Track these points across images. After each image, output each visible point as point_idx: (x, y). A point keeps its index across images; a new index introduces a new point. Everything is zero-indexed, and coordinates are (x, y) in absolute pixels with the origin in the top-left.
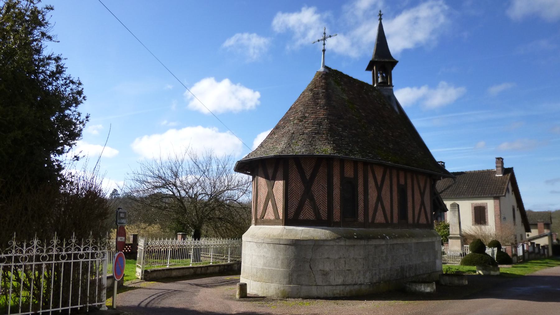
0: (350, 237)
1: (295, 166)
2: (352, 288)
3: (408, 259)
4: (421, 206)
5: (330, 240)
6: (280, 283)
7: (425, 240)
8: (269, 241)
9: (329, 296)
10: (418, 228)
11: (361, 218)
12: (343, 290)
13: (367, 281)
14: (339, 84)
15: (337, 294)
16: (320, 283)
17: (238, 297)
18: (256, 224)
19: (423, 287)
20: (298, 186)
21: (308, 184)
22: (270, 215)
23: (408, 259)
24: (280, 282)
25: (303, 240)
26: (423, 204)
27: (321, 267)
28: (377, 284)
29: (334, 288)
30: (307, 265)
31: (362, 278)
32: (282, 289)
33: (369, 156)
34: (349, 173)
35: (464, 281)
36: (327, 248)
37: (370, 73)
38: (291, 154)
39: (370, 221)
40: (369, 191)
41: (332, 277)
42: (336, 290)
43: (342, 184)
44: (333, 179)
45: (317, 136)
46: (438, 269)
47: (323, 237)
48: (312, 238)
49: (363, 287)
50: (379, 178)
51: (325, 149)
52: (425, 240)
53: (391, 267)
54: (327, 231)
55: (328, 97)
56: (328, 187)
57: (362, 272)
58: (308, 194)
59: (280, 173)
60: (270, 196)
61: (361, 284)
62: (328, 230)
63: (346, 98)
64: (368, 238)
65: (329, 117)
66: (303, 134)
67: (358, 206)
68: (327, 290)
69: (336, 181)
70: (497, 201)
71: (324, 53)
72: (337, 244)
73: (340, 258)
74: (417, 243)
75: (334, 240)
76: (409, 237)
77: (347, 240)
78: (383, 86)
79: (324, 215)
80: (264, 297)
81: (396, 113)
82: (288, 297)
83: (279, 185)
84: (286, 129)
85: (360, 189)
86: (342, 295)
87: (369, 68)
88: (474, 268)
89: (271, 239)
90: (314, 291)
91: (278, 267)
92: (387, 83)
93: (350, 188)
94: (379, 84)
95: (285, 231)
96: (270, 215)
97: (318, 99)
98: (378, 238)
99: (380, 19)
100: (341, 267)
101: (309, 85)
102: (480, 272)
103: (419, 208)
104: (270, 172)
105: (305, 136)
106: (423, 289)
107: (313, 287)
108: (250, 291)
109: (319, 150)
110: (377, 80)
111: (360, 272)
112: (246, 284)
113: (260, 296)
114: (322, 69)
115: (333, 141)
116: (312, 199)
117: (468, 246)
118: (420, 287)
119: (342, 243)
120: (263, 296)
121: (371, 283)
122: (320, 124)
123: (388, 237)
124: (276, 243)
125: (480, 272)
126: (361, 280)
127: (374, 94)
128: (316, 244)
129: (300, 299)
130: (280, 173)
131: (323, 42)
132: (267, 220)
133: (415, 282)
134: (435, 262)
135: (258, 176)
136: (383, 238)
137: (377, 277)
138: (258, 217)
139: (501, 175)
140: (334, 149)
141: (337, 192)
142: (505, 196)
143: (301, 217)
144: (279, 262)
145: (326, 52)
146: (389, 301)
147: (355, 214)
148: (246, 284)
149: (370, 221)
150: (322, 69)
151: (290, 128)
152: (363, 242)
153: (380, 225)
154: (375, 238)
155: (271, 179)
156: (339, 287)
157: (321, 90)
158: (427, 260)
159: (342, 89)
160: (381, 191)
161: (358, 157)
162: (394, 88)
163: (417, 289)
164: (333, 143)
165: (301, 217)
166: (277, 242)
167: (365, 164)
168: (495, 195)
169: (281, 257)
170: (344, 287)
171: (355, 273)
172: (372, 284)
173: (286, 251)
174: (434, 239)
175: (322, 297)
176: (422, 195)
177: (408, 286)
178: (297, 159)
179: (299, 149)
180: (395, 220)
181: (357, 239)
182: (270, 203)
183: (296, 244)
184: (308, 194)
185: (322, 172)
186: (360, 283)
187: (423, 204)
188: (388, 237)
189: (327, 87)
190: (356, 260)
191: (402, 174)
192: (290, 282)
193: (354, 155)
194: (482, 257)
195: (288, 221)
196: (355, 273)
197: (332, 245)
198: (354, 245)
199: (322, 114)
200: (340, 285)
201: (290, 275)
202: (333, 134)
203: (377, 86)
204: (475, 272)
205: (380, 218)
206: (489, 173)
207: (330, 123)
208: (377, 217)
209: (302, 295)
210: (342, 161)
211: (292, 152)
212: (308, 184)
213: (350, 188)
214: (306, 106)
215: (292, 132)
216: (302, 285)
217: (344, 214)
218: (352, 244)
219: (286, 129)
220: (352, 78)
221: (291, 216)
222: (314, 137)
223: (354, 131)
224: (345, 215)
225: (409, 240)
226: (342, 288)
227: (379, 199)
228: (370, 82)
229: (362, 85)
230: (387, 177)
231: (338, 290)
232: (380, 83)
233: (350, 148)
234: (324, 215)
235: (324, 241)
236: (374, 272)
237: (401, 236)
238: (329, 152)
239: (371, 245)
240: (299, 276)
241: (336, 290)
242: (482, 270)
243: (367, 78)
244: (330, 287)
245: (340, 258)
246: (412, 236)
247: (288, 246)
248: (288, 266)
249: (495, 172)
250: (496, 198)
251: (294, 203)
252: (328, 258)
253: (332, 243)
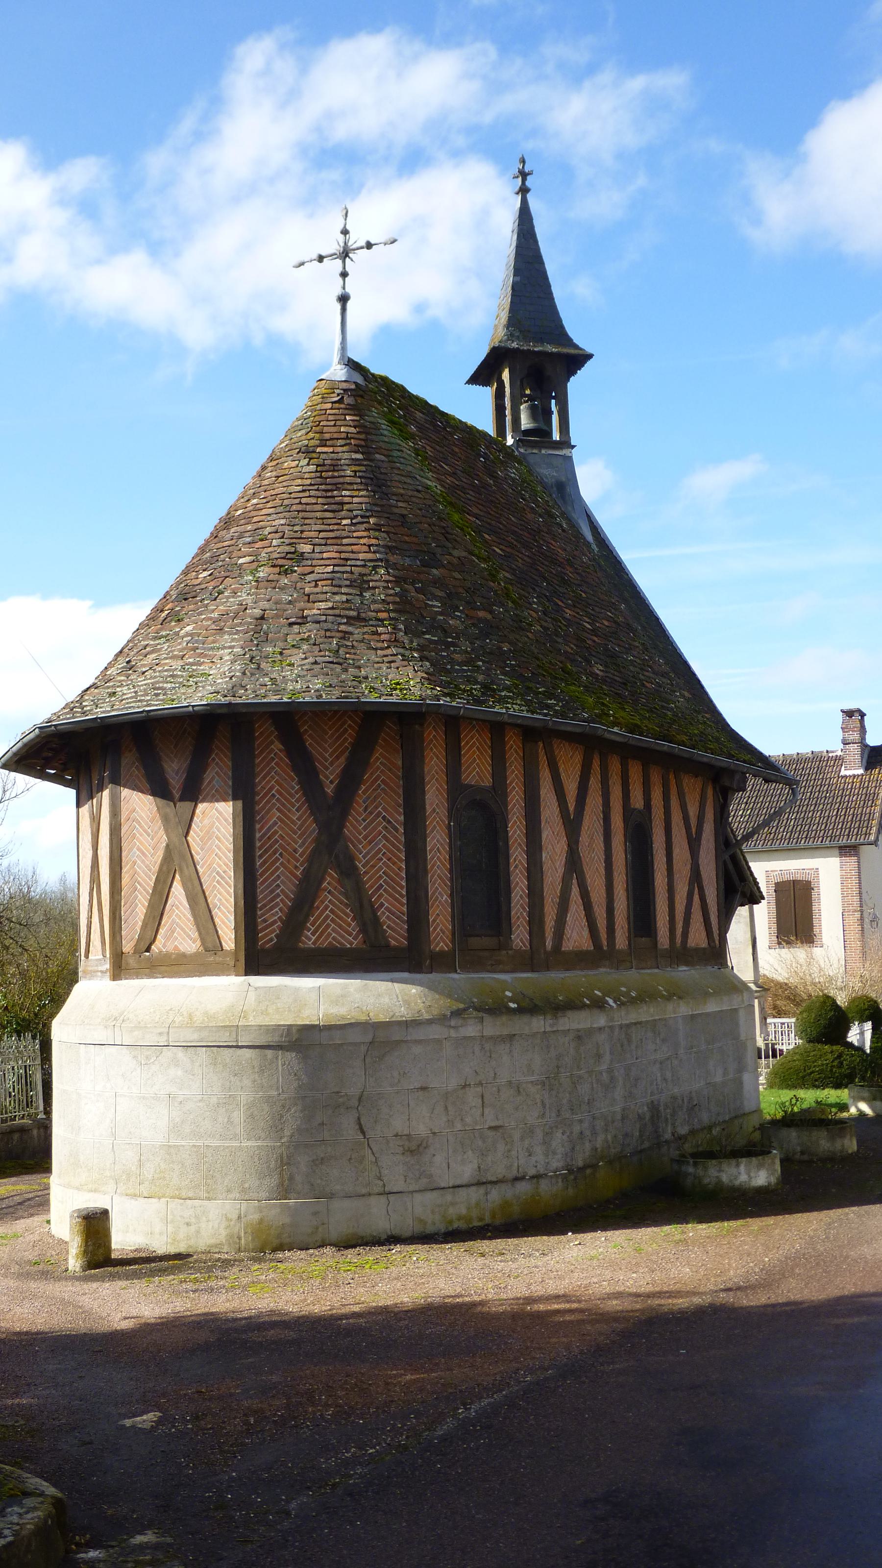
0: (495, 1008)
1: (277, 746)
2: (508, 1192)
3: (669, 1075)
4: (691, 884)
5: (430, 1022)
6: (245, 1194)
7: (712, 1007)
8: (192, 1037)
9: (430, 1229)
10: (687, 964)
11: (520, 937)
12: (478, 1204)
13: (557, 1163)
14: (408, 437)
15: (460, 1218)
16: (400, 1186)
17: (74, 1263)
18: (119, 968)
19: (742, 1168)
20: (292, 824)
21: (331, 813)
22: (179, 934)
23: (669, 1075)
24: (244, 1191)
25: (329, 1028)
26: (696, 877)
27: (399, 1124)
28: (588, 1171)
29: (449, 1198)
30: (348, 1122)
31: (539, 1156)
32: (256, 1217)
33: (548, 707)
34: (477, 771)
35: (846, 1142)
36: (417, 1050)
37: (486, 394)
38: (273, 699)
39: (549, 944)
40: (544, 836)
41: (438, 1159)
42: (453, 1204)
43: (453, 811)
44: (424, 793)
45: (357, 632)
46: (749, 1106)
47: (402, 1012)
48: (363, 1018)
49: (545, 1186)
50: (571, 788)
51: (397, 680)
52: (712, 1007)
53: (624, 1109)
54: (414, 990)
55: (376, 481)
56: (405, 824)
57: (539, 1134)
58: (332, 850)
59: (218, 771)
60: (177, 862)
61: (537, 1177)
62: (413, 983)
63: (438, 489)
64: (556, 1007)
65: (393, 559)
66: (302, 620)
67: (509, 892)
68: (424, 1209)
69: (435, 798)
70: (851, 862)
71: (344, 310)
72: (453, 1033)
73: (465, 1086)
74: (693, 1017)
75: (441, 1020)
76: (668, 998)
77: (488, 1019)
78: (534, 445)
79: (395, 932)
80: (179, 1256)
81: (588, 544)
82: (280, 1248)
83: (216, 823)
84: (228, 603)
85: (516, 829)
86: (476, 1223)
87: (484, 375)
88: (843, 1095)
89: (200, 1029)
90: (379, 1216)
91: (235, 1137)
92: (547, 439)
93: (481, 826)
94: (525, 438)
95: (252, 995)
96: (179, 934)
97: (338, 487)
98: (584, 1006)
99: (524, 191)
100: (468, 1120)
101: (294, 429)
102: (864, 1107)
103: (686, 888)
104: (175, 770)
105: (310, 630)
106: (743, 1178)
107: (373, 1200)
108: (123, 1239)
109: (377, 685)
110: (516, 421)
111: (531, 1131)
112: (105, 1213)
113: (161, 1251)
114: (338, 373)
115: (421, 649)
116: (348, 870)
117: (793, 1020)
118: (733, 1170)
119: (471, 1030)
120: (172, 1250)
121: (570, 1171)
122: (361, 584)
123: (611, 1001)
124: (221, 1043)
125: (864, 1107)
126: (538, 1160)
127: (513, 473)
128: (377, 1039)
129: (328, 1250)
130: (218, 771)
131: (339, 262)
132: (168, 955)
133: (710, 1155)
134: (741, 1083)
135: (116, 780)
136: (599, 1005)
137: (588, 1145)
138: (128, 947)
139: (861, 771)
140: (431, 679)
141: (437, 842)
142: (875, 843)
143: (309, 940)
144: (239, 1116)
145: (349, 304)
146: (655, 1229)
147: (497, 920)
148: (105, 1213)
149: (549, 944)
150: (338, 373)
151: (243, 596)
152: (539, 1024)
153: (580, 960)
154: (571, 1005)
155: (180, 793)
156: (463, 1192)
157: (345, 455)
158: (718, 1078)
159: (417, 452)
160: (579, 835)
161: (516, 710)
162: (575, 453)
163: (725, 1178)
164: (422, 658)
165: (309, 940)
166: (225, 1038)
167: (531, 734)
168: (844, 841)
169: (244, 1097)
170: (482, 1190)
171: (517, 1135)
172: (574, 1173)
173: (262, 1071)
174: (735, 1001)
175: (407, 1233)
176: (694, 844)
177: (691, 1170)
178: (288, 722)
179: (297, 679)
180: (621, 941)
181: (520, 1011)
182: (178, 890)
183: (302, 1043)
184: (332, 850)
185: (384, 765)
186: (532, 1172)
187: (696, 877)
188: (611, 1001)
189: (366, 442)
190: (518, 1089)
191: (635, 771)
192: (284, 1190)
193: (502, 701)
194: (840, 1056)
195: (257, 959)
196: (517, 1135)
197: (438, 1041)
198: (511, 1037)
199: (363, 545)
200: (468, 1186)
201: (285, 1162)
202: (414, 626)
203: (518, 442)
204: (844, 1107)
205: (577, 937)
206: (820, 762)
207: (398, 581)
208: (568, 931)
209: (334, 1236)
210: (453, 723)
211: (276, 692)
212: (331, 813)
213: (481, 826)
214: (299, 513)
215: (257, 612)
216: (331, 1196)
217: (463, 928)
218: (505, 1032)
219: (228, 603)
220: (436, 409)
221: (269, 936)
222: (346, 635)
223: (481, 614)
224: (469, 926)
225: (670, 1007)
226: (475, 1194)
227: (574, 863)
228: (485, 423)
229: (470, 433)
230: (594, 783)
231: (463, 1206)
232: (527, 432)
233: (481, 678)
234: (395, 932)
235: (407, 1024)
236: (577, 1129)
237: (645, 996)
238: (417, 691)
239: (566, 1032)
240: (318, 1162)
241: (453, 1204)
242: (869, 1101)
243: (475, 409)
244: (435, 1194)
245: (465, 1086)
246: (676, 993)
247: (269, 1053)
248: (276, 1127)
249: (839, 761)
250: (848, 850)
251: (279, 887)
252: (423, 1089)
253: (436, 1032)
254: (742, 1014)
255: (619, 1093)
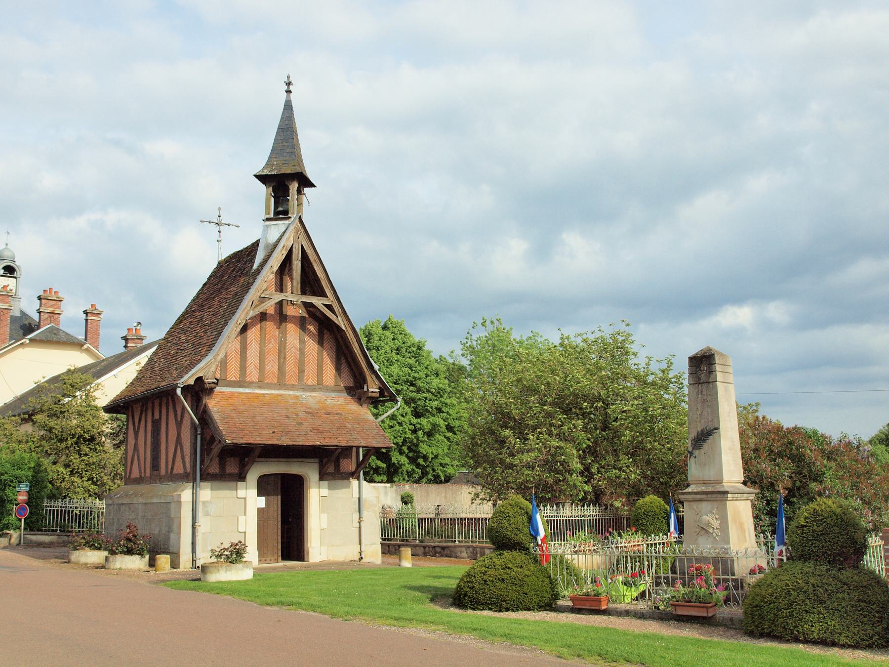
180: (148, 474)
254: (173, 505)
255: (115, 527)
